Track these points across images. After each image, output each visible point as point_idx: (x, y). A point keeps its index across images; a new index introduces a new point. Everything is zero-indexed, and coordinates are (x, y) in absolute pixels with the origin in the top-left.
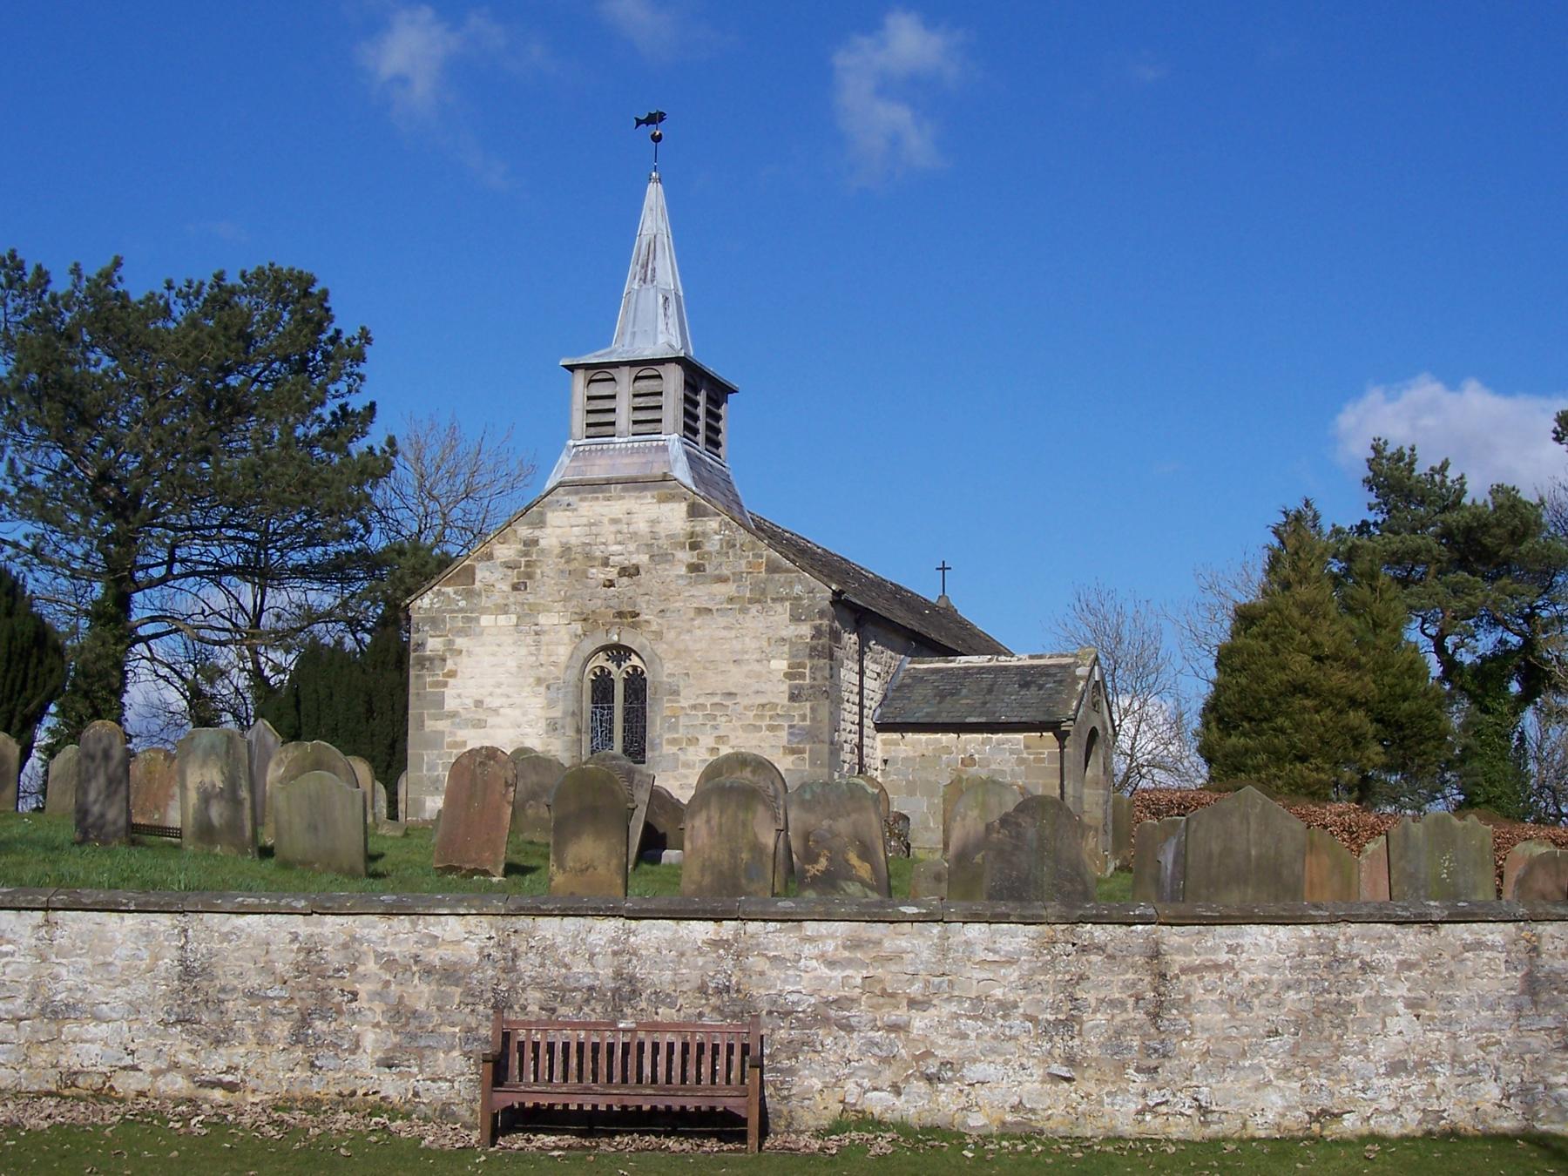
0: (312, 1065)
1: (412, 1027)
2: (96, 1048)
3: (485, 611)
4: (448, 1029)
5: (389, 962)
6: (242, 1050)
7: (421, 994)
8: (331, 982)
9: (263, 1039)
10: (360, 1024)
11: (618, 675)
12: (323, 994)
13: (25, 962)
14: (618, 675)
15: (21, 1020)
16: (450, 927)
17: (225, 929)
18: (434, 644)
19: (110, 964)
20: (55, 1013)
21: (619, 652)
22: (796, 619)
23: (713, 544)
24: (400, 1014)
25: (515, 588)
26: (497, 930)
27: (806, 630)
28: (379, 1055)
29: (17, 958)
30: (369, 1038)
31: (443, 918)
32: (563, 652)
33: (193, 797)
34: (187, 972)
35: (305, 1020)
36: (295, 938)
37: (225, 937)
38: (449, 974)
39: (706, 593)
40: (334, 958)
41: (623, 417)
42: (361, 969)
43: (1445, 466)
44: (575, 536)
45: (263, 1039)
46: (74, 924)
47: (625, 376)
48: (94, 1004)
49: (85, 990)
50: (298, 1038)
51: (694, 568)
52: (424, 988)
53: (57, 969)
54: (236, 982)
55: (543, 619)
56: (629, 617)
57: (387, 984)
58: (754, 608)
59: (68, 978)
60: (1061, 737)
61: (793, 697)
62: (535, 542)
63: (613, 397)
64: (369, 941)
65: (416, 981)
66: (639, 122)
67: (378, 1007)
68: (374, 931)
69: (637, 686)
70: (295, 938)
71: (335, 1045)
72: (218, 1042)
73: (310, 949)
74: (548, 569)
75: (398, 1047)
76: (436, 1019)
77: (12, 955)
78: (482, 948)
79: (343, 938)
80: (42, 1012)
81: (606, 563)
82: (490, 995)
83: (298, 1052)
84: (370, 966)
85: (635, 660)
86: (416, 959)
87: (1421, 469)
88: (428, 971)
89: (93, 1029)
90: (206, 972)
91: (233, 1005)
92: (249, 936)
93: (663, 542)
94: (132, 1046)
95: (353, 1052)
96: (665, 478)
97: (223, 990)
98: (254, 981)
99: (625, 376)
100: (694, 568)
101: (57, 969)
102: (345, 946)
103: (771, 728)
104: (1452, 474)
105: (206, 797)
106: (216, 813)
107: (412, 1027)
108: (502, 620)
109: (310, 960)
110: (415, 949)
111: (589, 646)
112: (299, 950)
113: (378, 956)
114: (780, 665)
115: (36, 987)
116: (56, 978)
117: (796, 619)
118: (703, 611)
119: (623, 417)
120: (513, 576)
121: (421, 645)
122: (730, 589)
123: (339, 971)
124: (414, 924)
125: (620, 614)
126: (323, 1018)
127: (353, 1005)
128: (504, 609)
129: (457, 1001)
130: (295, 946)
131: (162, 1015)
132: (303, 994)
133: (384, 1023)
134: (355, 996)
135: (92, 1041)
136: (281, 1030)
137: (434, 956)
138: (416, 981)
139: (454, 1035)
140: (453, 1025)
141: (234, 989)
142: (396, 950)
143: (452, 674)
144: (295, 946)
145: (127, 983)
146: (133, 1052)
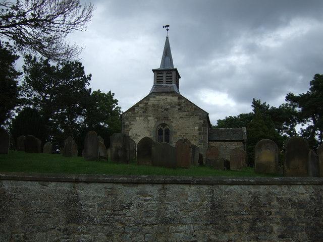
0: (257, 238)
1: (289, 224)
2: (181, 235)
3: (137, 117)
4: (301, 224)
5: (281, 201)
6: (233, 234)
7: (292, 212)
8: (262, 208)
9: (240, 230)
10: (273, 223)
11: (164, 129)
12: (260, 213)
13: (155, 203)
14: (164, 129)
15: (153, 225)
16: (300, 189)
17: (227, 190)
18: (127, 123)
19: (186, 203)
20: (166, 222)
21: (164, 125)
22: (200, 119)
23: (183, 104)
24: (286, 220)
25: (143, 112)
26: (315, 189)
27: (202, 121)
28: (279, 234)
29: (152, 202)
30: (275, 228)
31: (298, 186)
32: (153, 125)
33: (114, 149)
34: (214, 206)
35: (254, 222)
36: (250, 193)
37: (227, 193)
38: (300, 205)
39: (181, 114)
40: (263, 200)
41: (164, 80)
42: (272, 203)
43: (265, 103)
44: (156, 103)
45: (240, 230)
46: (174, 189)
47: (165, 73)
48: (181, 218)
49: (177, 213)
50: (252, 229)
51: (179, 109)
52: (293, 210)
53: (167, 205)
54: (230, 209)
55: (149, 118)
56: (166, 118)
57: (281, 209)
58: (192, 117)
59: (170, 210)
60: (244, 143)
61: (199, 134)
62: (148, 104)
63: (162, 77)
64: (275, 194)
65: (290, 207)
66: (164, 27)
67: (278, 217)
68: (276, 190)
69: (167, 132)
70: (250, 193)
71: (265, 231)
72: (225, 231)
73: (255, 197)
74: (150, 109)
75: (285, 231)
76: (297, 221)
77: (151, 201)
78: (311, 196)
79: (266, 193)
80: (161, 222)
81: (162, 108)
82: (314, 212)
83: (252, 234)
84: (275, 202)
85: (167, 127)
86: (290, 200)
87: (261, 103)
88: (294, 204)
89: (180, 228)
90: (220, 206)
91: (230, 217)
92: (235, 192)
93: (173, 104)
94: (194, 234)
95: (270, 233)
96: (173, 92)
97: (226, 212)
98: (236, 209)
99: (165, 73)
100: (179, 109)
101: (167, 205)
102: (267, 196)
103: (195, 140)
104: (266, 104)
105: (117, 150)
106: (120, 154)
107: (289, 224)
108: (141, 118)
109: (255, 200)
110: (289, 196)
111: (159, 124)
112: (252, 197)
113: (278, 199)
114: (197, 128)
115: (159, 212)
116: (166, 209)
117: (200, 119)
118: (180, 117)
119: (164, 80)
120: (143, 110)
121: (124, 123)
122: (187, 113)
123: (264, 204)
124: (289, 188)
125: (165, 118)
126: (260, 221)
127: (270, 216)
128: (141, 116)
129: (304, 214)
130: (250, 196)
131: (206, 222)
132: (253, 213)
133: (280, 223)
134: (270, 213)
135: (180, 232)
136: (246, 226)
137: (295, 199)
138: (290, 207)
139: (303, 226)
140: (303, 223)
141: (230, 212)
142: (283, 197)
143: (131, 129)
144: (250, 196)
145: (192, 210)
146: (195, 236)
